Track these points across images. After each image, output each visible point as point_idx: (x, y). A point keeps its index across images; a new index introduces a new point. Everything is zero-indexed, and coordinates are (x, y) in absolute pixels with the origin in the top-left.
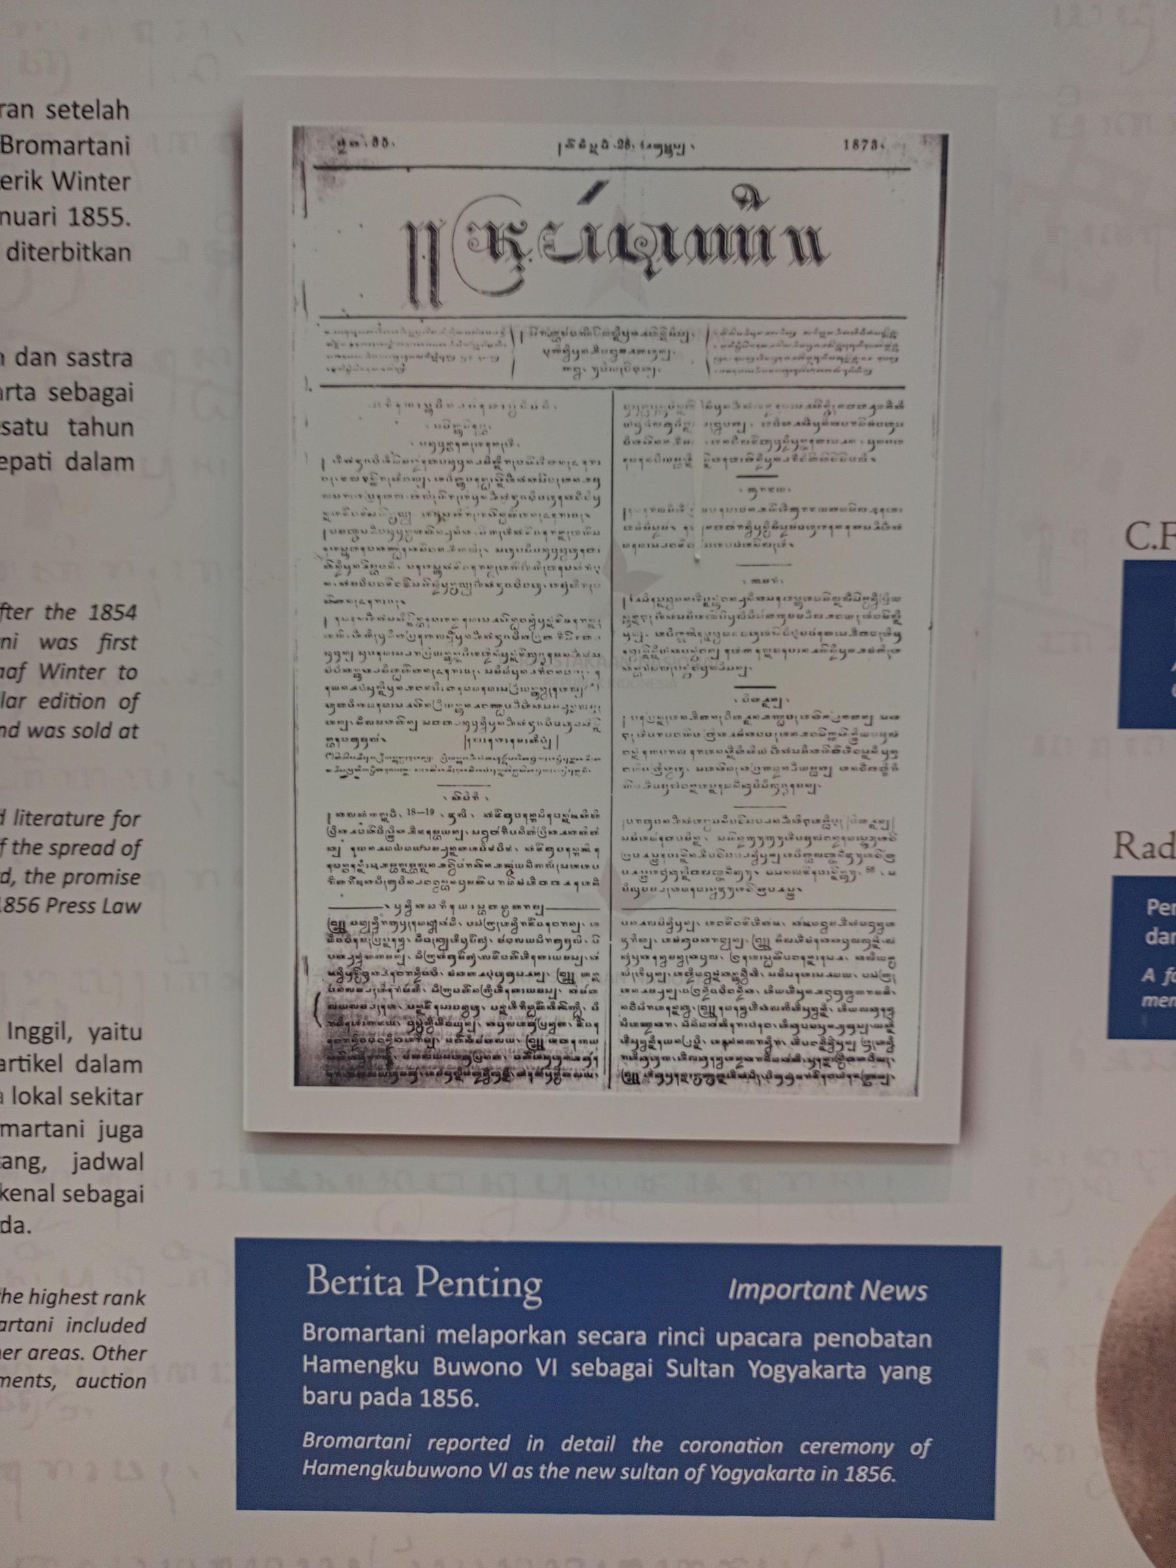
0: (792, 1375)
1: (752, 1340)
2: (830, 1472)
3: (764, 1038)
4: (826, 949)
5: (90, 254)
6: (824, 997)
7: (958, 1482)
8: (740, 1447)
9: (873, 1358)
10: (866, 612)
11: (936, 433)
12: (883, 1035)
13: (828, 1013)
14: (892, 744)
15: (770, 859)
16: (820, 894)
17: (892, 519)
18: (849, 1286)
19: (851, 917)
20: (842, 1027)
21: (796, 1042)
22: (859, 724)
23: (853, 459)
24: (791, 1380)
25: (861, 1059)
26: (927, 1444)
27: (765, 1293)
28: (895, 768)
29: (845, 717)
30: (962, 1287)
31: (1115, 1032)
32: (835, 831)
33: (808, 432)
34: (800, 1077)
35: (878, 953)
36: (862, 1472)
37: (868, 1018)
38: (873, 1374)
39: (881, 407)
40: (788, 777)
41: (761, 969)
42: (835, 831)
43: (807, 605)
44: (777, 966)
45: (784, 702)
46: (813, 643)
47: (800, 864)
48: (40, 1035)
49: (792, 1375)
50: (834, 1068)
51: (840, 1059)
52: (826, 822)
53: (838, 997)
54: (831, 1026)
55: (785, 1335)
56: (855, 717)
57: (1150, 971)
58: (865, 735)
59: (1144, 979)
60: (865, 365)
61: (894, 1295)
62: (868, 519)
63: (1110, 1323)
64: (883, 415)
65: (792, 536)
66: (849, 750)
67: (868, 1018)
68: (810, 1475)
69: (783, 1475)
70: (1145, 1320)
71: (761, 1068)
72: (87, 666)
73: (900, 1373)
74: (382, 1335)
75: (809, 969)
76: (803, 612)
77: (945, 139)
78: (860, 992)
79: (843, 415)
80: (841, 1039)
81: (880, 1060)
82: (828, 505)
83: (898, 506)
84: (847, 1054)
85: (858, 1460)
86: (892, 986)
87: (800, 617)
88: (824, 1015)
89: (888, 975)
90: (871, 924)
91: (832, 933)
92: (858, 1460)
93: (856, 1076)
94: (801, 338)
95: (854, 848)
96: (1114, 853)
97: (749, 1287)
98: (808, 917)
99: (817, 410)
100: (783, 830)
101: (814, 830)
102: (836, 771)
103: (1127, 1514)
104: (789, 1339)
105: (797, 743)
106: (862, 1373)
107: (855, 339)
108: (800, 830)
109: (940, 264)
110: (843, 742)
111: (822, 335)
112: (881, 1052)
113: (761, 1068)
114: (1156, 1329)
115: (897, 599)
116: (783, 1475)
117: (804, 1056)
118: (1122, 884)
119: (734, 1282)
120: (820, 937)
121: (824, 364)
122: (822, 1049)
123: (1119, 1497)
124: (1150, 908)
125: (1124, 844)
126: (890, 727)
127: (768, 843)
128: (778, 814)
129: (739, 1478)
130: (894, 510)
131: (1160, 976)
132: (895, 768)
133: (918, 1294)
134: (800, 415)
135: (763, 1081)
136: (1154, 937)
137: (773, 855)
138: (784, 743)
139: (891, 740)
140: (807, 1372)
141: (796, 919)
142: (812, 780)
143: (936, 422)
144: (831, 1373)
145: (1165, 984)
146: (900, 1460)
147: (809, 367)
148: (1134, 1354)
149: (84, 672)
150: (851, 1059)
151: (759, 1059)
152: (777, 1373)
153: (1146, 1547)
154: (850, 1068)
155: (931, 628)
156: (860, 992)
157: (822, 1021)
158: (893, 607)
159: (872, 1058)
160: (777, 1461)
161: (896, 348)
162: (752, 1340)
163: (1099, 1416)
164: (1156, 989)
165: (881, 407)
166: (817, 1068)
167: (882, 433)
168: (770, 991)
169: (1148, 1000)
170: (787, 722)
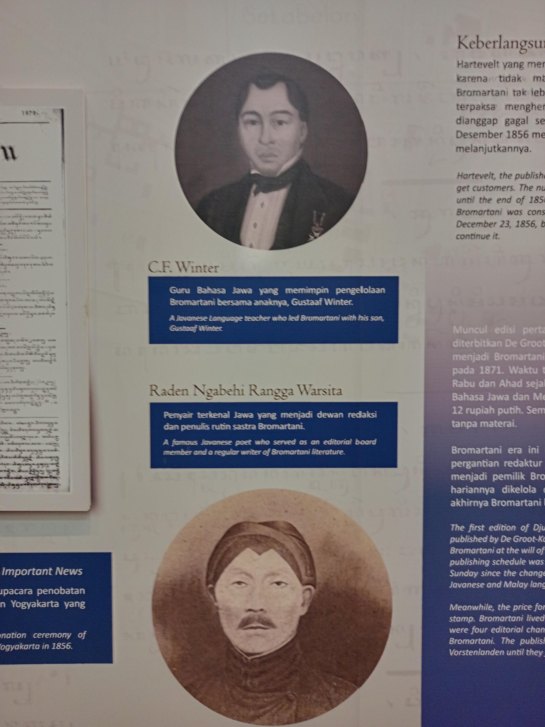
0: (29, 606)
1: (13, 592)
2: (46, 645)
3: (6, 469)
4: (31, 433)
5: (496, 149)
6: (30, 453)
7: (96, 648)
8: (9, 636)
9: (61, 599)
10: (40, 298)
11: (64, 227)
12: (54, 467)
13: (32, 459)
14: (53, 351)
15: (6, 397)
16: (27, 411)
17: (49, 261)
18: (51, 569)
19: (40, 420)
20: (38, 464)
21: (20, 471)
22: (40, 343)
23: (32, 238)
24: (29, 608)
25: (46, 477)
26: (85, 633)
27: (16, 573)
28: (55, 361)
29: (34, 340)
30: (96, 569)
31: (153, 466)
32: (32, 386)
33: (13, 227)
34: (22, 485)
35: (51, 435)
36: (59, 645)
37: (48, 461)
38: (62, 605)
39: (42, 217)
40: (12, 365)
41: (5, 442)
42: (32, 386)
43: (17, 296)
44: (11, 440)
45: (9, 335)
46: (20, 311)
47: (18, 399)
48: (481, 122)
49: (29, 606)
50: (35, 481)
51: (38, 477)
52: (28, 383)
53: (36, 453)
54: (34, 464)
55: (25, 590)
56: (38, 340)
57: (166, 440)
58: (42, 347)
59: (164, 444)
60: (34, 200)
61: (68, 573)
62: (39, 261)
63: (157, 583)
64: (43, 220)
65: (9, 268)
66: (36, 354)
67: (48, 461)
68: (37, 647)
69: (27, 647)
70: (171, 581)
71: (6, 481)
72: (476, 173)
73: (73, 605)
74: (50, 604)
75: (24, 441)
76: (15, 299)
77: (62, 111)
78: (45, 451)
79: (26, 220)
80: (37, 469)
81: (54, 478)
82: (23, 256)
83: (51, 256)
84: (40, 475)
85: (57, 640)
86: (58, 448)
87: (14, 300)
88: (30, 460)
89: (55, 444)
90: (47, 423)
91: (33, 427)
92: (57, 640)
93: (45, 484)
94: (9, 190)
95: (40, 392)
96: (249, 393)
97: (10, 571)
98: (23, 420)
99: (16, 218)
100: (11, 386)
101: (24, 386)
102: (31, 362)
103: (166, 659)
104: (27, 591)
105: (15, 351)
106: (57, 605)
107: (30, 190)
108: (18, 386)
109: (63, 160)
110: (33, 350)
111: (17, 188)
112: (54, 474)
113: (6, 481)
114: (175, 585)
115: (52, 293)
116: (27, 647)
117: (23, 476)
118: (153, 406)
119: (4, 569)
120: (27, 428)
121: (19, 200)
122: (30, 473)
123: (162, 653)
124: (165, 416)
125: (153, 390)
126: (52, 344)
127: (5, 391)
128: (8, 379)
129: (9, 649)
130: (50, 258)
131: (170, 442)
132: (55, 361)
133: (78, 572)
134: (10, 220)
135: (7, 487)
136: (168, 427)
137: (7, 396)
138: (10, 351)
139: (52, 349)
140: (35, 604)
141: (18, 422)
142: (22, 366)
143: (64, 223)
144: (45, 605)
145: (172, 446)
146: (74, 640)
147: (12, 201)
148: (166, 595)
149: (474, 176)
150: (42, 477)
151: (5, 478)
152: (23, 605)
153: (174, 673)
154: (42, 481)
155: (66, 305)
156: (45, 451)
157: (30, 462)
158: (51, 296)
159: (51, 477)
160: (24, 641)
161: (47, 193)
162: (13, 592)
163: (154, 620)
164: (169, 448)
165: (42, 217)
166: (28, 481)
167: (43, 227)
168: (8, 450)
169: (166, 452)
170: (10, 342)
